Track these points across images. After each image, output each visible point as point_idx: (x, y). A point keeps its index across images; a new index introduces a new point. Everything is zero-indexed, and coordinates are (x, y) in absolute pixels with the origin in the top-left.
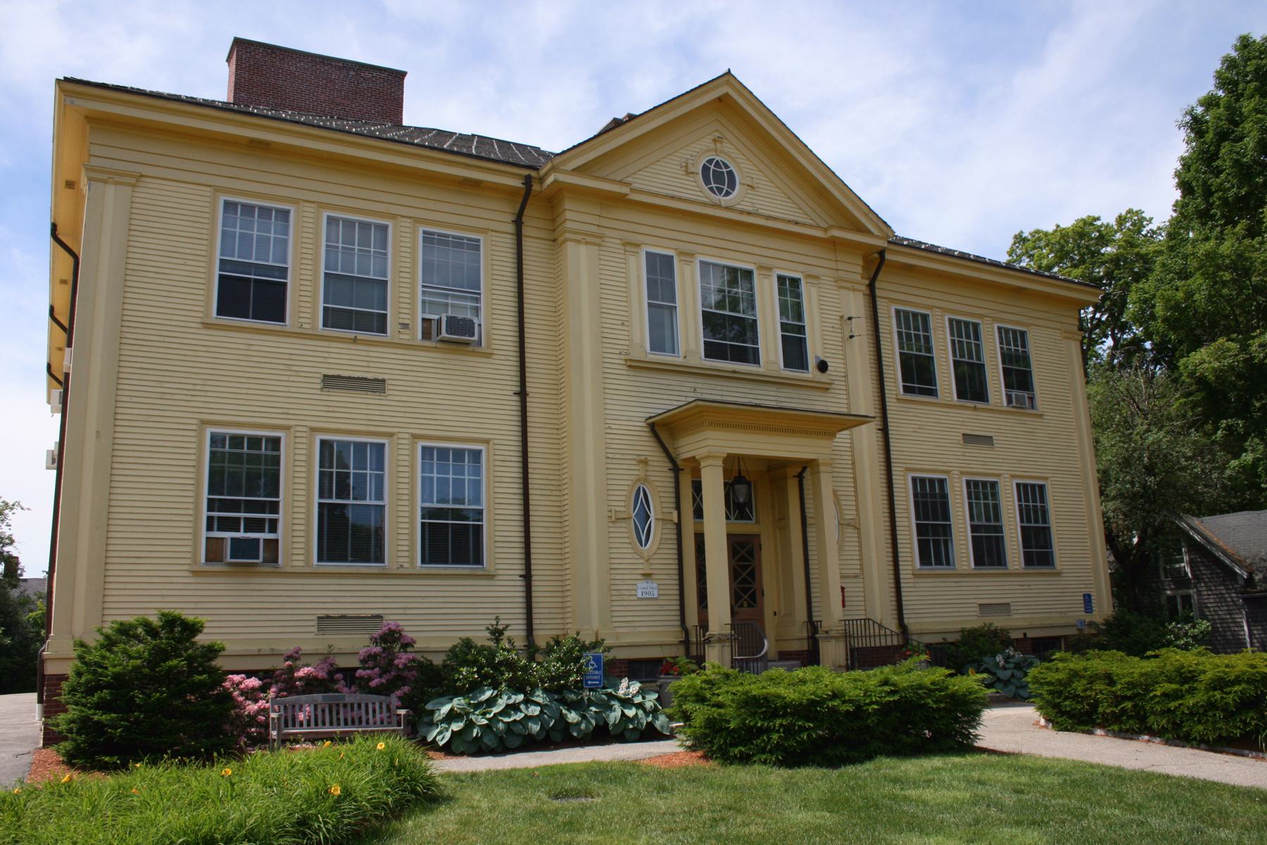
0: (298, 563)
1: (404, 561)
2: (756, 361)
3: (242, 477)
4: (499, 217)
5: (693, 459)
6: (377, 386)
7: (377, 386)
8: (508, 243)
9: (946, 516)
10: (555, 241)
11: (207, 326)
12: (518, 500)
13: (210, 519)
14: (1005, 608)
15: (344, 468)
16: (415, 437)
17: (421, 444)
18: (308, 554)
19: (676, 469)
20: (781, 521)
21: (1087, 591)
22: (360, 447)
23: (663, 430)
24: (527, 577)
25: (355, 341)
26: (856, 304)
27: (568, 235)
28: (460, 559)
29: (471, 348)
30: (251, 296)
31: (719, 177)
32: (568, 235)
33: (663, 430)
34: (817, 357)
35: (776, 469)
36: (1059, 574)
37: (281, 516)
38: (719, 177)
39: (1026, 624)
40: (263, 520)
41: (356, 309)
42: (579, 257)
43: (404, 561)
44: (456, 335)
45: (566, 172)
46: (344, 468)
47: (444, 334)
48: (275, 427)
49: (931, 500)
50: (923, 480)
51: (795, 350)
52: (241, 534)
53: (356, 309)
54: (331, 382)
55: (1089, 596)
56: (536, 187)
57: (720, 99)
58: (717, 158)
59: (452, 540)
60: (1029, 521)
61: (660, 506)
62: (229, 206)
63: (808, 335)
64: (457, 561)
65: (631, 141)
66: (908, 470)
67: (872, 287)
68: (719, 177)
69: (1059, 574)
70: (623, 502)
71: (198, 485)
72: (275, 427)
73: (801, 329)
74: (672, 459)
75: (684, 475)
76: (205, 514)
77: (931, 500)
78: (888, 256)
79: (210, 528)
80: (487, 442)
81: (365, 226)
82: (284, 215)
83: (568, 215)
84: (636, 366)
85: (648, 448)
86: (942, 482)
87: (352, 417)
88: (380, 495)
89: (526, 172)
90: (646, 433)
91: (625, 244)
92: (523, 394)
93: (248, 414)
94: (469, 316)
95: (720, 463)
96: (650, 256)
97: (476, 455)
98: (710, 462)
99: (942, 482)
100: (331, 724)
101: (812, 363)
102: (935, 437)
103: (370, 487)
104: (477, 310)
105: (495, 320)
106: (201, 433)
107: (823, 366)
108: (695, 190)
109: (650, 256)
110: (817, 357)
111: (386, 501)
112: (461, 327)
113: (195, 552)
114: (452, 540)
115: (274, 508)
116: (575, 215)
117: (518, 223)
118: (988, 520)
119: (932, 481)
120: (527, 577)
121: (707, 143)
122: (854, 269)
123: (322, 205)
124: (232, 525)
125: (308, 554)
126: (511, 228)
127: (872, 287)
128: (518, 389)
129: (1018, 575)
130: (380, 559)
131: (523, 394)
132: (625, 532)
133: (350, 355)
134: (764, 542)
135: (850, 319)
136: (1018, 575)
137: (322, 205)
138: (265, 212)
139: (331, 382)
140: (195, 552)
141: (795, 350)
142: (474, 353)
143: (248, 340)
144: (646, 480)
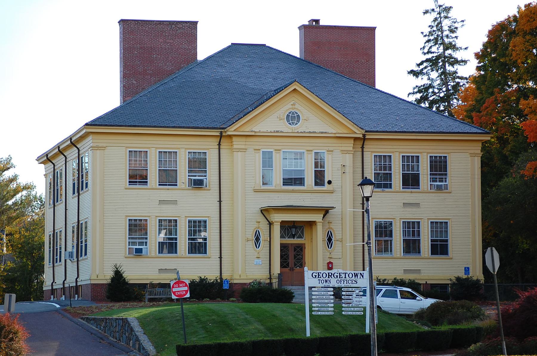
0: (153, 254)
1: (183, 253)
4: (214, 142)
6: (175, 202)
11: (126, 189)
14: (418, 271)
15: (412, 228)
16: (428, 219)
17: (402, 221)
21: (467, 266)
22: (413, 222)
25: (411, 192)
28: (442, 254)
30: (138, 178)
37: (148, 241)
39: (427, 278)
41: (168, 178)
43: (183, 253)
46: (412, 228)
48: (145, 216)
52: (138, 247)
53: (168, 178)
54: (161, 202)
55: (468, 268)
56: (224, 134)
59: (198, 248)
60: (409, 236)
64: (200, 253)
65: (325, 111)
72: (145, 216)
76: (128, 240)
78: (367, 137)
79: (129, 245)
81: (385, 156)
93: (137, 213)
97: (176, 221)
102: (391, 206)
103: (173, 232)
106: (185, 220)
108: (285, 128)
113: (126, 252)
114: (198, 248)
117: (219, 145)
118: (413, 235)
123: (157, 148)
124: (134, 244)
125: (156, 253)
128: (218, 200)
130: (176, 253)
132: (252, 244)
133: (167, 193)
137: (157, 148)
140: (126, 252)
141: (319, 178)
142: (202, 190)
143: (138, 191)
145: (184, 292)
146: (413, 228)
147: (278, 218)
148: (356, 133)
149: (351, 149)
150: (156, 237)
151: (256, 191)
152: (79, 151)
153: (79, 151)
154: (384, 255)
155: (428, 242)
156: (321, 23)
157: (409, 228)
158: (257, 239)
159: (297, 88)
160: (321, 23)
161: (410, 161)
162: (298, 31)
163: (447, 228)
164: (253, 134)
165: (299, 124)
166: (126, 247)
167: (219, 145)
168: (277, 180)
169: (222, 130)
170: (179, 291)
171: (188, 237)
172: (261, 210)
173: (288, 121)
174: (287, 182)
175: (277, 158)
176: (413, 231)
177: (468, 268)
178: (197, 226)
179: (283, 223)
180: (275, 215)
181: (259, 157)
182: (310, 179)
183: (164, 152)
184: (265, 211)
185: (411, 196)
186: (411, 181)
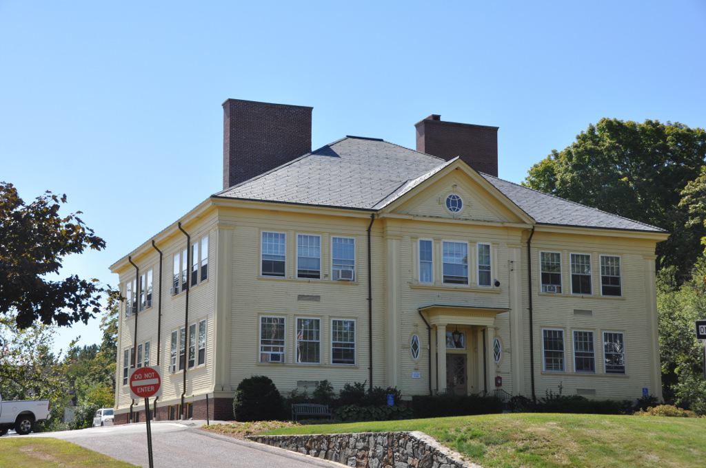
2: (467, 283)
3: (272, 332)
5: (434, 325)
6: (316, 298)
7: (316, 298)
8: (365, 239)
9: (562, 348)
10: (383, 235)
12: (367, 340)
13: (262, 347)
15: (310, 329)
16: (330, 317)
18: (572, 369)
19: (429, 328)
20: (475, 349)
21: (646, 387)
23: (424, 313)
24: (371, 369)
26: (517, 255)
27: (388, 237)
29: (350, 282)
30: (273, 268)
31: (454, 203)
32: (388, 237)
33: (424, 313)
34: (495, 280)
35: (474, 329)
36: (628, 377)
37: (285, 346)
38: (454, 203)
40: (270, 347)
41: (309, 273)
42: (393, 245)
44: (346, 277)
45: (387, 213)
46: (310, 329)
47: (340, 278)
49: (553, 342)
50: (550, 332)
51: (485, 278)
54: (301, 297)
56: (376, 217)
57: (457, 169)
58: (454, 194)
60: (581, 348)
61: (422, 343)
62: (265, 234)
63: (491, 271)
66: (541, 327)
67: (529, 243)
68: (454, 203)
69: (628, 377)
70: (407, 340)
71: (258, 335)
73: (489, 268)
74: (428, 325)
75: (431, 328)
76: (260, 345)
77: (553, 342)
78: (536, 230)
79: (262, 350)
80: (356, 318)
82: (283, 236)
83: (389, 228)
84: (413, 288)
85: (419, 320)
86: (561, 333)
87: (309, 310)
88: (318, 338)
89: (371, 213)
90: (417, 313)
91: (412, 238)
92: (370, 299)
94: (349, 269)
95: (445, 327)
96: (422, 242)
98: (441, 327)
99: (561, 333)
100: (427, 280)
101: (492, 282)
103: (315, 336)
104: (353, 267)
105: (360, 270)
107: (497, 284)
108: (444, 211)
109: (422, 242)
110: (495, 280)
111: (320, 341)
112: (347, 274)
114: (344, 355)
115: (282, 343)
116: (392, 228)
117: (369, 231)
118: (586, 349)
119: (555, 332)
120: (371, 369)
121: (450, 188)
122: (517, 238)
124: (267, 349)
125: (572, 369)
126: (366, 233)
127: (529, 243)
128: (368, 297)
129: (601, 376)
130: (318, 362)
131: (370, 299)
133: (307, 287)
134: (468, 357)
135: (512, 262)
136: (601, 376)
138: (276, 235)
139: (301, 297)
140: (258, 359)
141: (485, 278)
142: (351, 284)
144: (417, 332)
145: (153, 388)
146: (586, 339)
147: (443, 320)
148: (524, 223)
149: (519, 242)
150: (292, 340)
151: (413, 288)
152: (161, 254)
153: (161, 254)
154: (554, 371)
155: (572, 356)
156: (442, 119)
157: (581, 339)
158: (415, 347)
159: (462, 167)
160: (442, 119)
161: (581, 261)
162: (415, 128)
163: (591, 339)
164: (411, 217)
165: (460, 210)
166: (258, 352)
167: (369, 231)
168: (438, 274)
169: (375, 213)
170: (142, 386)
171: (332, 342)
172: (420, 312)
173: (448, 206)
174: (448, 280)
175: (437, 251)
176: (586, 344)
177: (647, 389)
178: (343, 331)
179: (449, 328)
180: (441, 316)
181: (417, 247)
182: (473, 275)
183: (310, 236)
184: (424, 313)
185: (581, 301)
186: (582, 285)
